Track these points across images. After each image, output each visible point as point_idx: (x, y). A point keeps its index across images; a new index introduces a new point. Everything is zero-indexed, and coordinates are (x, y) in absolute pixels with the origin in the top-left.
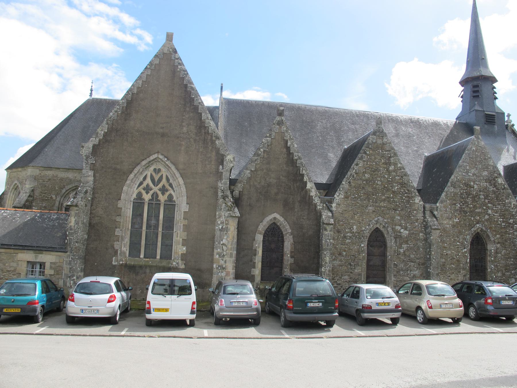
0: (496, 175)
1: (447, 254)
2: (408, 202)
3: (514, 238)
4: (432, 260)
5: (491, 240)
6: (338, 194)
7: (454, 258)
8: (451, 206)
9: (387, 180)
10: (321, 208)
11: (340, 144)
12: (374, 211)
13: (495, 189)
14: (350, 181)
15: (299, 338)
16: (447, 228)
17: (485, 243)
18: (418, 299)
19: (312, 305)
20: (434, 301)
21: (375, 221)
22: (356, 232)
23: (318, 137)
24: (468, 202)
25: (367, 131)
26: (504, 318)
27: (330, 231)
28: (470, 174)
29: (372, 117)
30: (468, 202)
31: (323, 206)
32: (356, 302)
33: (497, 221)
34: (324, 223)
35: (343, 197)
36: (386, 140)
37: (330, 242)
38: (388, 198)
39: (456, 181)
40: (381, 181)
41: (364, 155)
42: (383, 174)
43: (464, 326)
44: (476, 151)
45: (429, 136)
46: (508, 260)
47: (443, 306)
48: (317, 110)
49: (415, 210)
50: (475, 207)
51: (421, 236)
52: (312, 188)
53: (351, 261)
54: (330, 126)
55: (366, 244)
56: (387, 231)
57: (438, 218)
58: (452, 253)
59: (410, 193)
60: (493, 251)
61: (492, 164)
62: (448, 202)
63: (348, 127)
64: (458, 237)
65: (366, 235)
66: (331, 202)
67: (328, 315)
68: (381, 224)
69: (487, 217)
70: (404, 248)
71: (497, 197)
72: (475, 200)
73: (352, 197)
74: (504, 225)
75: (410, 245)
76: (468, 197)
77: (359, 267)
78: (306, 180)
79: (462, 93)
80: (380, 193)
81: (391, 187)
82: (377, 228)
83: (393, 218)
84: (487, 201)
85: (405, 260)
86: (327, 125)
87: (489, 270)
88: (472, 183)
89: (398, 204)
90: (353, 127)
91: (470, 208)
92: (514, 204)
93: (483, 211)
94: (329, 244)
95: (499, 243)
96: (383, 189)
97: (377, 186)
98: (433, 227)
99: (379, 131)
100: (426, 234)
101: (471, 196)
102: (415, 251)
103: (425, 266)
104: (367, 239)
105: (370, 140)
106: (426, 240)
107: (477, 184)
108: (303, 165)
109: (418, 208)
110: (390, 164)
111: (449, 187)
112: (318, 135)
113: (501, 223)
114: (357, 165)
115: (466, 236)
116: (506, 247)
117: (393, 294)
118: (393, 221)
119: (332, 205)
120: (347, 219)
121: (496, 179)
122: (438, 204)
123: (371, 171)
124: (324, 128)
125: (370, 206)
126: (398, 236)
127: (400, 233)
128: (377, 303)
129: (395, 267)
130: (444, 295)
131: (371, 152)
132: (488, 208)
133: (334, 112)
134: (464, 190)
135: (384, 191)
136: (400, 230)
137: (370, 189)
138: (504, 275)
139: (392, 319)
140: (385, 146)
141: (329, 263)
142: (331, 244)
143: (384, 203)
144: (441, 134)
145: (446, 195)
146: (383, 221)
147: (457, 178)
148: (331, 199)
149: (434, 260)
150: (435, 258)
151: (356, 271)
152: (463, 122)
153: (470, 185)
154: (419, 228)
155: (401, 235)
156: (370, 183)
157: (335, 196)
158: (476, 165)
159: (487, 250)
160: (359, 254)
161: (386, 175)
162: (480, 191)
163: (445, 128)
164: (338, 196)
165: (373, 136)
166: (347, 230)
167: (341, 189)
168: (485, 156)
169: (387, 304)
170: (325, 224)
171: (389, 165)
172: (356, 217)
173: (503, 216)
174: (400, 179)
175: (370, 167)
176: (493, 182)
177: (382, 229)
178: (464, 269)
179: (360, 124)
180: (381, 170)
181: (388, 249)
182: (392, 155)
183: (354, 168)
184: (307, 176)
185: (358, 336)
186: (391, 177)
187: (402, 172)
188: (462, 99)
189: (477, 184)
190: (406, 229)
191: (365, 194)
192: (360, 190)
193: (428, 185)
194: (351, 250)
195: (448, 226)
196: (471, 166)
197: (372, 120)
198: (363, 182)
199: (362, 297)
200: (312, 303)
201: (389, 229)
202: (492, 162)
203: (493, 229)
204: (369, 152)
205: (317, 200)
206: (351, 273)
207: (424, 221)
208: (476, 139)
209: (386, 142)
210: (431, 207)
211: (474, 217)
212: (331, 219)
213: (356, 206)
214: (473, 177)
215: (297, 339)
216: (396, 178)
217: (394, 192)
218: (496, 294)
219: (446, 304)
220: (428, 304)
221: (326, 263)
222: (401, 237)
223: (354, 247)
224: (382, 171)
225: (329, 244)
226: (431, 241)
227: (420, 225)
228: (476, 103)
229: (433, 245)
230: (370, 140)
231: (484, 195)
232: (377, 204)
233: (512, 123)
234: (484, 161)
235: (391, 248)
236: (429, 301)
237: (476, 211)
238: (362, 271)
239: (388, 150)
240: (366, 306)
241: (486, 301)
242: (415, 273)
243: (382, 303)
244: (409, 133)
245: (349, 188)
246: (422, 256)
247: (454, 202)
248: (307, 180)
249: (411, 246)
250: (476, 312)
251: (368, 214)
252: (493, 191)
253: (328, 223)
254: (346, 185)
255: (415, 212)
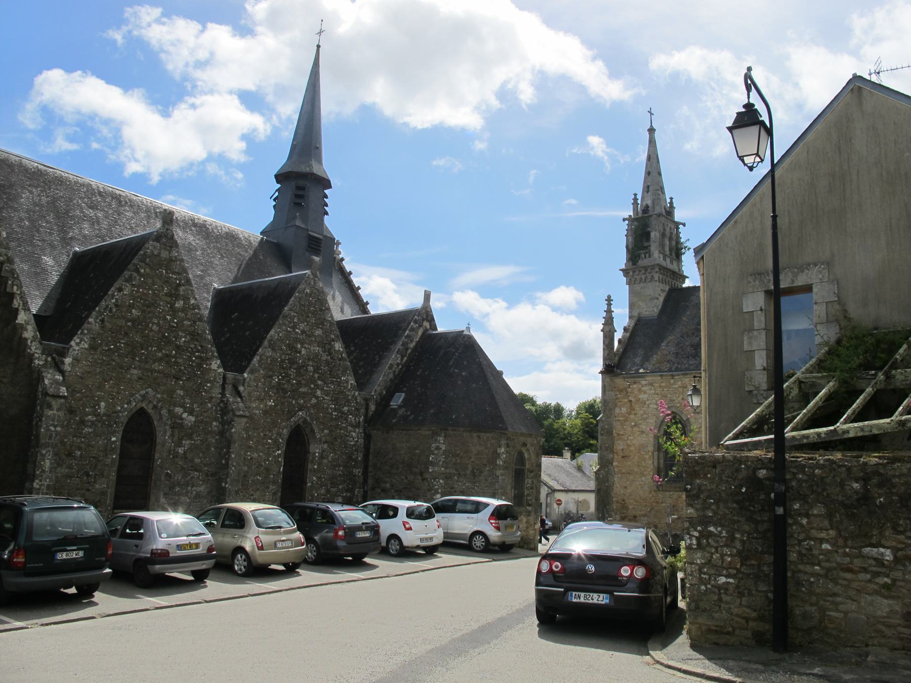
0: (333, 336)
1: (251, 459)
2: (200, 366)
3: (347, 436)
4: (231, 468)
5: (315, 438)
6: (78, 341)
7: (262, 465)
8: (264, 379)
9: (170, 324)
10: (41, 363)
11: (66, 241)
12: (140, 378)
13: (329, 358)
14: (103, 319)
15: (47, 625)
16: (255, 414)
17: (307, 441)
18: (238, 535)
19: (64, 557)
20: (266, 538)
21: (140, 395)
22: (104, 414)
23: (22, 220)
24: (291, 375)
25: (117, 225)
26: (350, 558)
27: (58, 410)
28: (297, 330)
29: (126, 203)
30: (291, 375)
31: (46, 360)
32: (137, 546)
33: (327, 409)
34: (46, 394)
35: (86, 346)
36: (177, 254)
37: (55, 431)
38: (167, 356)
39: (277, 339)
40: (158, 324)
41: (135, 274)
42: (163, 313)
43: (306, 576)
44: (310, 295)
45: (222, 255)
46: (335, 470)
47: (279, 545)
48: (20, 165)
49: (210, 382)
50: (299, 384)
51: (215, 426)
52: (28, 324)
53: (90, 468)
54: (48, 203)
55: (120, 436)
56: (160, 415)
57: (244, 398)
58: (259, 456)
59: (205, 351)
60: (317, 454)
61: (330, 319)
62: (262, 371)
63: (83, 212)
64: (270, 431)
65: (122, 419)
66: (63, 354)
67: (89, 574)
68: (150, 402)
69: (314, 401)
70: (185, 447)
71: (331, 371)
72: (300, 372)
73: (104, 348)
74: (336, 415)
75: (195, 441)
76: (290, 367)
77: (104, 479)
78: (16, 307)
79: (277, 194)
80: (155, 347)
81: (175, 337)
82: (142, 409)
83: (171, 393)
84: (316, 375)
85: (185, 466)
86: (40, 200)
87: (309, 484)
88: (299, 346)
89: (183, 368)
90: (91, 213)
91: (293, 385)
92: (351, 384)
93: (310, 391)
94: (54, 435)
95: (326, 442)
96: (161, 339)
97: (151, 334)
98: (238, 413)
99: (166, 236)
100: (223, 423)
101: (295, 366)
102: (203, 453)
103: (217, 477)
104: (123, 428)
105: (148, 248)
106: (222, 433)
107: (305, 348)
108: (14, 275)
109: (215, 379)
110: (177, 297)
111: (266, 348)
112: (23, 215)
113: (332, 412)
114: (120, 290)
115: (283, 429)
116: (334, 450)
117: (205, 530)
118: (172, 398)
119: (64, 359)
120: (90, 390)
121: (333, 343)
122: (246, 375)
123: (143, 305)
124: (35, 204)
125: (135, 368)
126: (177, 425)
127: (182, 419)
128: (178, 546)
129: (168, 478)
130: (280, 527)
131: (148, 270)
132: (317, 386)
133: (56, 177)
134: (286, 354)
135: (163, 343)
136: (182, 414)
137: (138, 338)
138: (328, 491)
139: (194, 573)
140: (173, 263)
141: (50, 472)
142: (56, 435)
143: (160, 365)
144: (240, 255)
145: (260, 361)
146: (154, 397)
147: (278, 335)
148: (64, 348)
149: (233, 468)
150: (235, 464)
151: (97, 486)
152: (273, 241)
153: (296, 348)
154: (212, 413)
155: (182, 423)
156: (140, 327)
157: (73, 343)
158: (308, 317)
159: (309, 452)
160: (106, 454)
161: (168, 315)
162: (309, 359)
163: (246, 245)
164: (78, 344)
165: (155, 243)
166: (87, 409)
167: (86, 332)
168: (322, 304)
169: (194, 547)
170: (50, 395)
171: (176, 298)
172: (107, 386)
173: (335, 400)
174: (191, 325)
175: (143, 297)
176: (327, 347)
177: (150, 411)
178: (274, 483)
179: (104, 211)
180: (160, 305)
181: (158, 448)
182: (183, 281)
183: (113, 296)
184: (21, 298)
185: (157, 606)
186: (175, 321)
187: (197, 314)
188: (274, 203)
189: (305, 348)
190: (191, 413)
191: (128, 345)
192: (121, 336)
193: (222, 340)
194: (92, 447)
195: (257, 412)
196: (301, 317)
197: (127, 208)
198: (126, 323)
199: (149, 535)
200: (65, 553)
201: (164, 412)
202: (329, 315)
203: (321, 420)
204: (145, 270)
205: (35, 348)
206: (88, 490)
207: (222, 401)
208: (312, 277)
209: (176, 257)
210: (235, 379)
211: (296, 400)
212: (61, 388)
213: (109, 367)
214: (301, 337)
215: (42, 627)
216: (185, 322)
217: (178, 348)
218: (351, 522)
219: (283, 541)
220: (257, 543)
221: (43, 471)
222: (181, 426)
223: (98, 442)
224: (162, 307)
225: (54, 435)
226: (231, 436)
227: (214, 408)
228: (298, 214)
229: (235, 443)
230: (148, 248)
231: (313, 366)
232: (147, 366)
233: (341, 256)
234: (319, 312)
235: (163, 445)
236: (258, 537)
237: (300, 390)
238: (108, 487)
239: (176, 272)
240: (159, 551)
241: (336, 533)
242: (199, 489)
243: (187, 545)
244: (190, 243)
245: (101, 332)
246: (213, 460)
247: (270, 373)
248: (19, 306)
249: (196, 442)
250: (318, 550)
251: (129, 383)
252: (326, 360)
253: (55, 394)
254: (95, 325)
255: (208, 385)
